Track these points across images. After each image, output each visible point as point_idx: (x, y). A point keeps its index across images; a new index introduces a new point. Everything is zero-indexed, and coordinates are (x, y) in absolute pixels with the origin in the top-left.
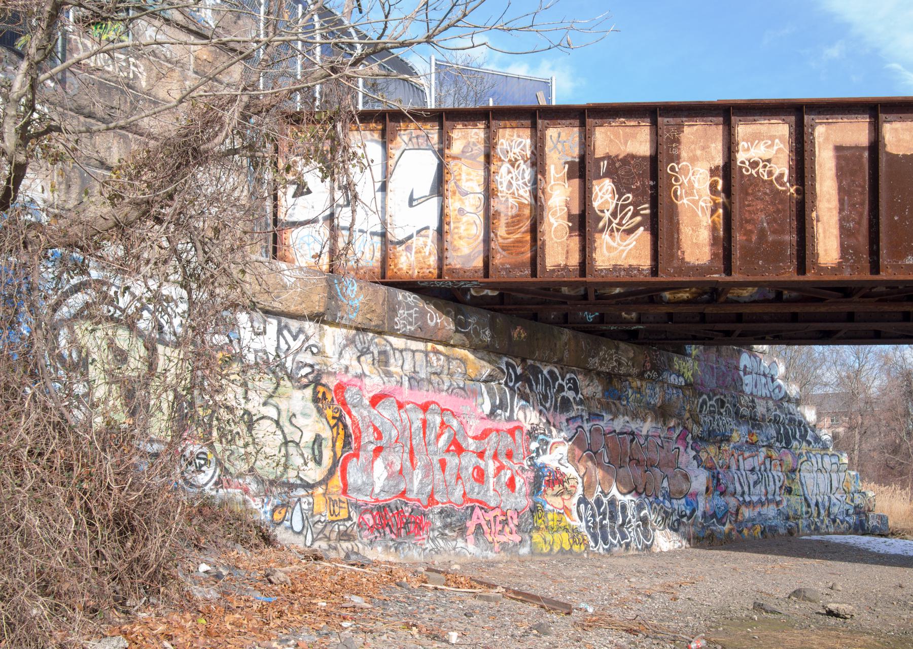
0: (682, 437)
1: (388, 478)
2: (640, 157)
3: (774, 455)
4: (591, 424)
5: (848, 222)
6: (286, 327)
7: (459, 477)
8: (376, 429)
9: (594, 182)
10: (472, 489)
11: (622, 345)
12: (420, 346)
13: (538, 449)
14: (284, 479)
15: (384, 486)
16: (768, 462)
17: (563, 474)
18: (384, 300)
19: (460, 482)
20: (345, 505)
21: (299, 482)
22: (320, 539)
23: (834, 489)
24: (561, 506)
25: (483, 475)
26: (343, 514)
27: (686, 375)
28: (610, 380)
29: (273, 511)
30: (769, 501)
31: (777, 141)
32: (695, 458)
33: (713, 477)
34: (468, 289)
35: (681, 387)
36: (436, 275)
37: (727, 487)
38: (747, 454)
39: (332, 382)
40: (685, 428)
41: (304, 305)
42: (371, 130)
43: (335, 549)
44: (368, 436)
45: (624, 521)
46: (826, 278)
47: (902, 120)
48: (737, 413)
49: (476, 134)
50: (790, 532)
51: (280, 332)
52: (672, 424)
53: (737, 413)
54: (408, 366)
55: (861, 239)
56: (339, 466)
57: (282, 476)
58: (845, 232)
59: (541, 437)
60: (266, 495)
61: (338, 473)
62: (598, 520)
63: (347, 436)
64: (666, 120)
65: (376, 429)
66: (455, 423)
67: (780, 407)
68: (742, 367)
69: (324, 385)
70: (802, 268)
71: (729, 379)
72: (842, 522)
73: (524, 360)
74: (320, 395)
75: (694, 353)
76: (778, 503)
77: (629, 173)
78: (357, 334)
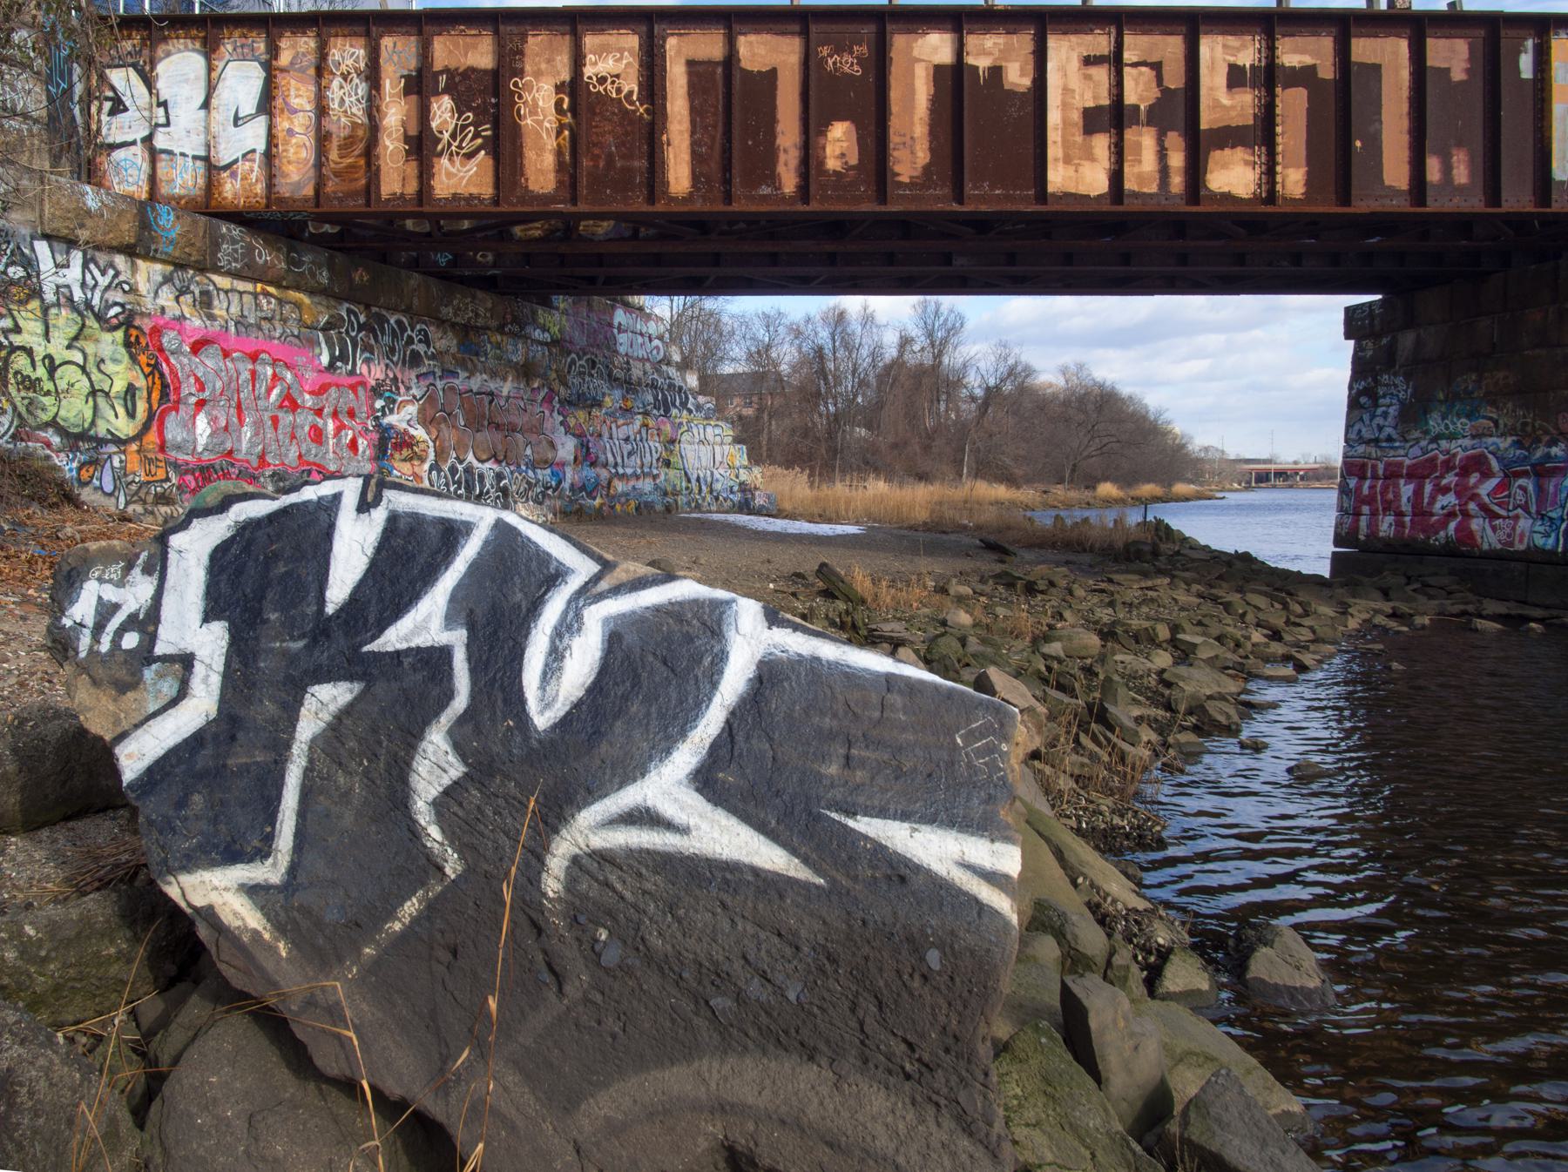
0: (548, 400)
1: (211, 435)
2: (481, 70)
3: (651, 423)
4: (444, 382)
5: (700, 146)
6: (93, 260)
7: (293, 437)
8: (197, 379)
9: (433, 99)
10: (309, 451)
11: (480, 294)
12: (249, 287)
13: (383, 407)
14: (92, 432)
15: (207, 444)
16: (644, 431)
17: (412, 437)
18: (205, 232)
19: (294, 442)
20: (163, 464)
21: (109, 437)
22: (135, 502)
23: (717, 464)
24: (410, 472)
25: (321, 434)
26: (161, 474)
27: (552, 330)
28: (466, 333)
29: (79, 469)
30: (645, 475)
31: (626, 53)
32: (562, 423)
33: (582, 445)
34: (305, 223)
35: (546, 344)
36: (263, 205)
37: (597, 457)
38: (621, 422)
39: (146, 324)
40: (551, 390)
41: (111, 235)
42: (191, 38)
43: (152, 513)
44: (188, 387)
45: (481, 492)
46: (674, 208)
47: (757, 32)
48: (610, 375)
49: (306, 43)
50: (668, 509)
51: (85, 266)
52: (536, 385)
53: (610, 375)
54: (234, 310)
55: (713, 165)
56: (155, 420)
57: (89, 429)
58: (697, 158)
59: (387, 394)
60: (71, 451)
61: (154, 428)
62: (452, 489)
63: (165, 386)
64: (509, 28)
65: (197, 379)
66: (289, 376)
67: (658, 371)
68: (616, 324)
69: (137, 328)
70: (651, 199)
71: (601, 337)
72: (725, 500)
73: (368, 307)
74: (133, 339)
75: (562, 306)
76: (655, 477)
77: (469, 88)
78: (175, 270)
